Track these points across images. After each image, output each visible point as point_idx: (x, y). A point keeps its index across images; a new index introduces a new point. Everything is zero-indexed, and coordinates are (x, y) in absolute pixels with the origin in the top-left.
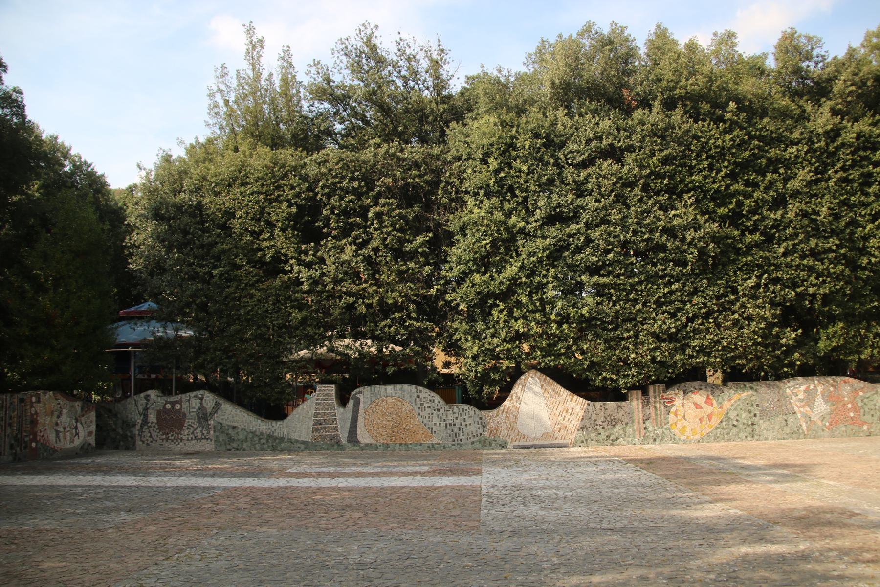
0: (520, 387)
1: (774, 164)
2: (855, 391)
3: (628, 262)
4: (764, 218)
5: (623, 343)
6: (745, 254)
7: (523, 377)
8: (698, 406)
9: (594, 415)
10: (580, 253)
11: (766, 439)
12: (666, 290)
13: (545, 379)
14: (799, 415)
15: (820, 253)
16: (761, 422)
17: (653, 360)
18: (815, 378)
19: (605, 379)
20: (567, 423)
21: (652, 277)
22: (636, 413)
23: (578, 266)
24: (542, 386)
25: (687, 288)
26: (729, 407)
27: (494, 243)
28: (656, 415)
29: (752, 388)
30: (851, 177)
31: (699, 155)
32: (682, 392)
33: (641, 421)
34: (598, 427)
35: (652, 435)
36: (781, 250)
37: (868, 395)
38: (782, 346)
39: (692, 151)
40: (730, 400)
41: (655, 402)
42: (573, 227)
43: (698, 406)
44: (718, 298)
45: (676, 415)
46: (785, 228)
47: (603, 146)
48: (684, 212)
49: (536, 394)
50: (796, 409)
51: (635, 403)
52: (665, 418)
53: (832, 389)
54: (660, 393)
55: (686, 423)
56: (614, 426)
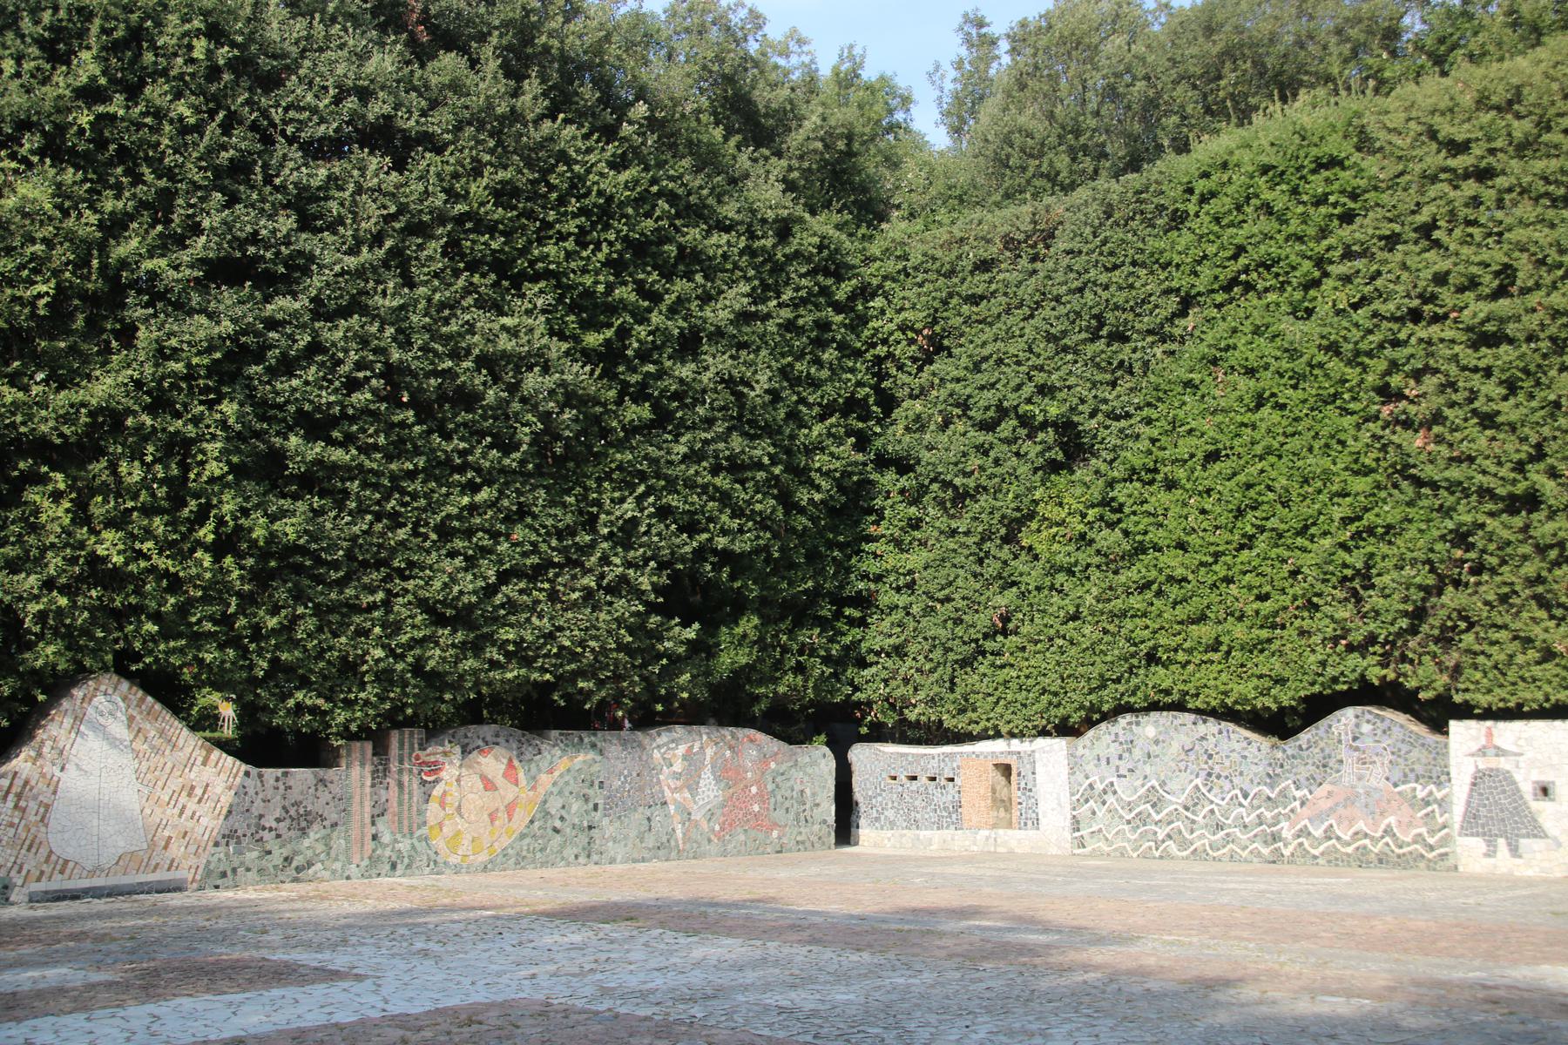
0: (68, 722)
1: (691, 259)
2: (765, 758)
3: (396, 419)
4: (661, 374)
5: (357, 619)
6: (620, 445)
7: (78, 693)
8: (489, 785)
9: (258, 802)
10: (291, 375)
11: (612, 861)
12: (466, 500)
13: (142, 700)
14: (672, 808)
15: (744, 467)
16: (606, 821)
17: (418, 668)
18: (703, 729)
19: (300, 709)
20: (190, 824)
21: (440, 463)
22: (357, 799)
23: (281, 407)
24: (131, 719)
25: (506, 503)
26: (549, 787)
27: (62, 293)
28: (400, 803)
29: (594, 746)
30: (801, 322)
31: (562, 201)
32: (458, 749)
33: (368, 820)
34: (266, 835)
35: (388, 853)
36: (683, 449)
37: (783, 767)
38: (660, 656)
39: (551, 188)
40: (551, 772)
41: (400, 771)
42: (283, 304)
43: (489, 785)
44: (560, 535)
45: (443, 805)
46: (696, 402)
47: (371, 117)
48: (523, 323)
49: (113, 742)
50: (667, 793)
51: (354, 774)
52: (420, 812)
53: (728, 753)
54: (412, 748)
55: (461, 824)
56: (304, 832)
